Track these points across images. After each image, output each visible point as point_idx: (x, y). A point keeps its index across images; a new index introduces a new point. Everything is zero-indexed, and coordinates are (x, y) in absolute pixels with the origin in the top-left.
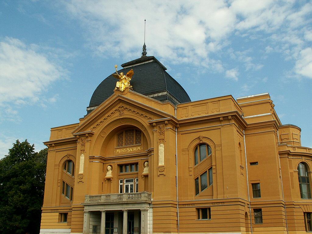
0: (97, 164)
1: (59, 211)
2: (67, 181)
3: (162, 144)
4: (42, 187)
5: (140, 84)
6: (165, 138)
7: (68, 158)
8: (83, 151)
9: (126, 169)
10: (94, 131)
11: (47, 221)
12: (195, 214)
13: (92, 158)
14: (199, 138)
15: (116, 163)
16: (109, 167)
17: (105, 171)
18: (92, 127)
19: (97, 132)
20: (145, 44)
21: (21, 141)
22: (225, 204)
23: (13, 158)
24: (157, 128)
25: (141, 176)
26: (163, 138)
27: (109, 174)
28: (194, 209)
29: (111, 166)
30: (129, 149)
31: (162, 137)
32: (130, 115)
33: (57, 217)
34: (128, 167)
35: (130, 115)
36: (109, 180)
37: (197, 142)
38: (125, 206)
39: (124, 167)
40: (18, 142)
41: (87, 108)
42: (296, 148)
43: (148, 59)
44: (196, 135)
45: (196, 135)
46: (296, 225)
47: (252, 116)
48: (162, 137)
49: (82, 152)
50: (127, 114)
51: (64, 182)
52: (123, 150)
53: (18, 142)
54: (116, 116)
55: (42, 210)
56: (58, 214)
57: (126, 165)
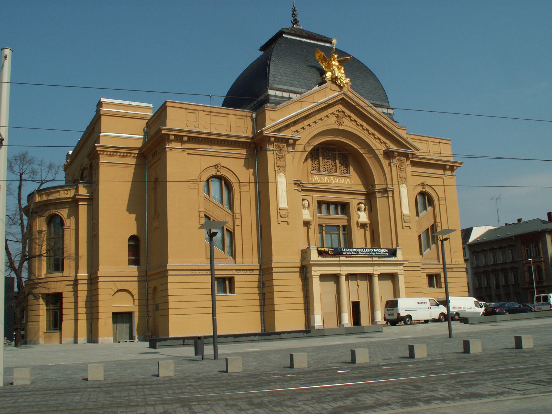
2: (221, 214)
3: (282, 174)
6: (287, 165)
7: (218, 171)
8: (282, 168)
11: (179, 292)
12: (426, 280)
14: (216, 166)
15: (315, 198)
22: (454, 270)
25: (357, 223)
26: (405, 176)
28: (424, 275)
30: (334, 179)
31: (281, 163)
32: (352, 128)
34: (332, 207)
35: (352, 128)
37: (213, 172)
38: (344, 268)
39: (324, 207)
43: (325, 39)
44: (213, 161)
45: (213, 161)
48: (281, 163)
50: (348, 125)
52: (327, 180)
54: (331, 123)
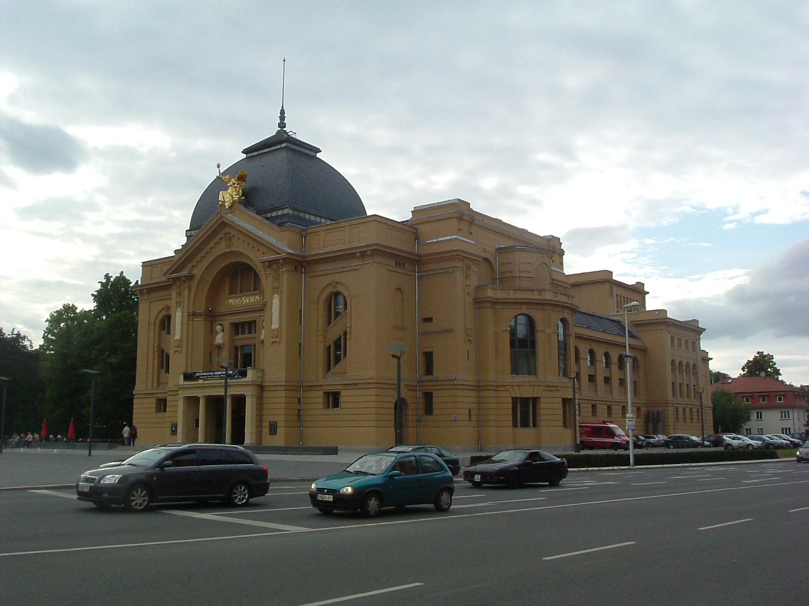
0: (200, 324)
1: (156, 395)
4: (134, 361)
5: (269, 184)
9: (243, 329)
10: (195, 272)
13: (194, 314)
16: (218, 328)
17: (212, 332)
18: (190, 265)
19: (198, 272)
20: (283, 107)
21: (114, 275)
22: (359, 386)
23: (179, 269)
24: (271, 269)
27: (219, 339)
29: (221, 325)
33: (154, 405)
36: (219, 347)
40: (107, 277)
41: (187, 231)
42: (558, 295)
46: (373, 405)
47: (462, 239)
49: (178, 304)
51: (163, 351)
53: (107, 277)
55: (134, 395)
56: (154, 400)
57: (243, 324)
